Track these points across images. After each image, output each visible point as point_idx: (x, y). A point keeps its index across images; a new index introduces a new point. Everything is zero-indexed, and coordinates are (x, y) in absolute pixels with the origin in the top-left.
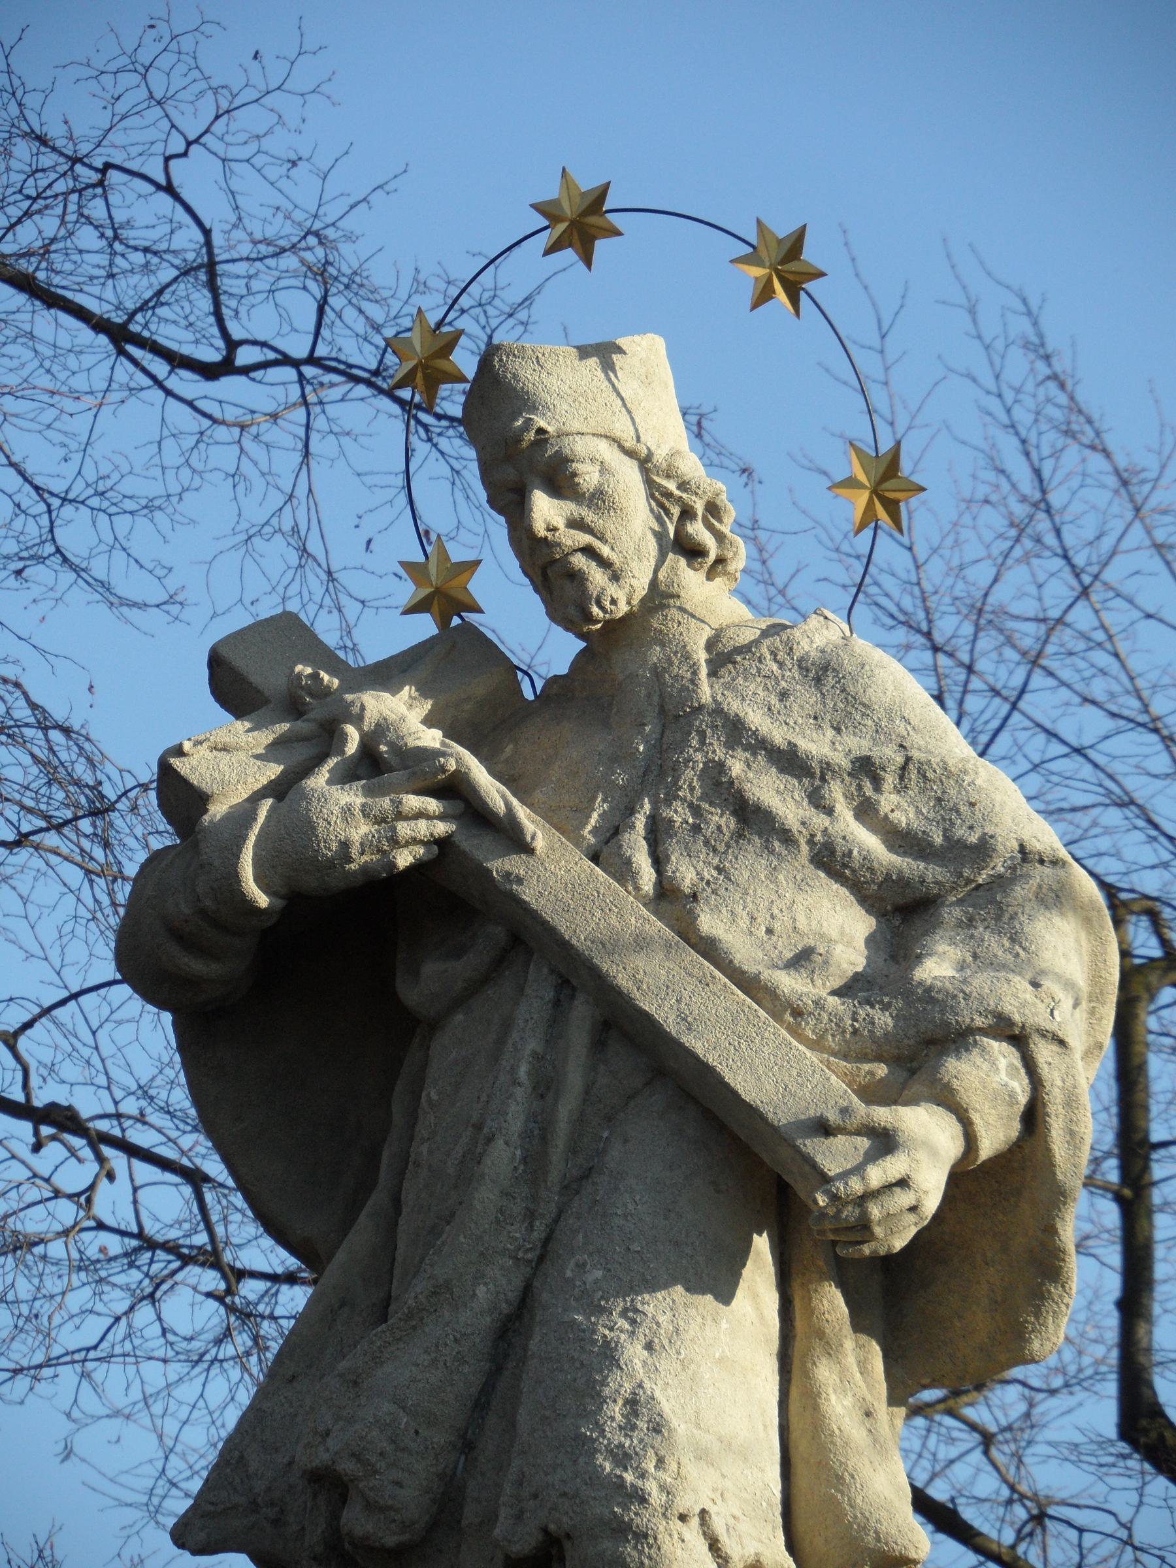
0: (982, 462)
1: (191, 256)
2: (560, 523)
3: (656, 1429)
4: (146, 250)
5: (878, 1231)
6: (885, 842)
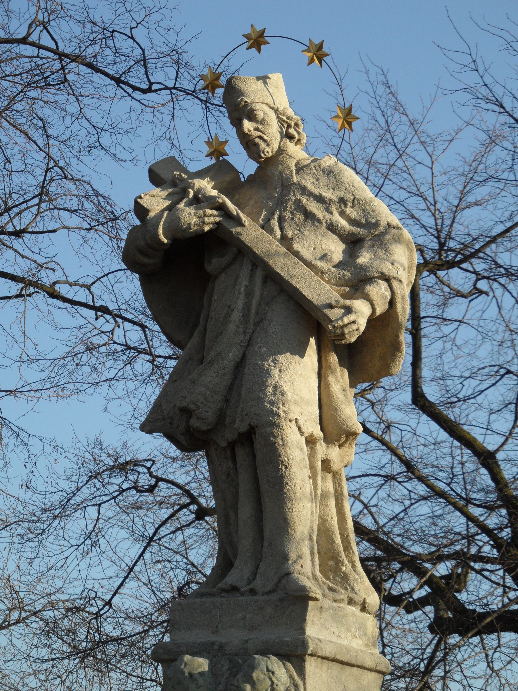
0: (370, 118)
1: (138, 57)
2: (252, 129)
3: (282, 395)
4: (125, 56)
5: (347, 336)
6: (348, 222)
